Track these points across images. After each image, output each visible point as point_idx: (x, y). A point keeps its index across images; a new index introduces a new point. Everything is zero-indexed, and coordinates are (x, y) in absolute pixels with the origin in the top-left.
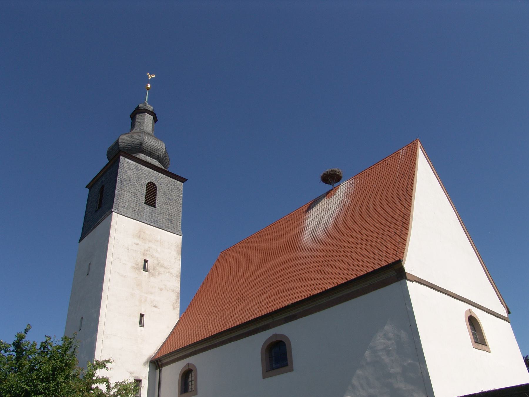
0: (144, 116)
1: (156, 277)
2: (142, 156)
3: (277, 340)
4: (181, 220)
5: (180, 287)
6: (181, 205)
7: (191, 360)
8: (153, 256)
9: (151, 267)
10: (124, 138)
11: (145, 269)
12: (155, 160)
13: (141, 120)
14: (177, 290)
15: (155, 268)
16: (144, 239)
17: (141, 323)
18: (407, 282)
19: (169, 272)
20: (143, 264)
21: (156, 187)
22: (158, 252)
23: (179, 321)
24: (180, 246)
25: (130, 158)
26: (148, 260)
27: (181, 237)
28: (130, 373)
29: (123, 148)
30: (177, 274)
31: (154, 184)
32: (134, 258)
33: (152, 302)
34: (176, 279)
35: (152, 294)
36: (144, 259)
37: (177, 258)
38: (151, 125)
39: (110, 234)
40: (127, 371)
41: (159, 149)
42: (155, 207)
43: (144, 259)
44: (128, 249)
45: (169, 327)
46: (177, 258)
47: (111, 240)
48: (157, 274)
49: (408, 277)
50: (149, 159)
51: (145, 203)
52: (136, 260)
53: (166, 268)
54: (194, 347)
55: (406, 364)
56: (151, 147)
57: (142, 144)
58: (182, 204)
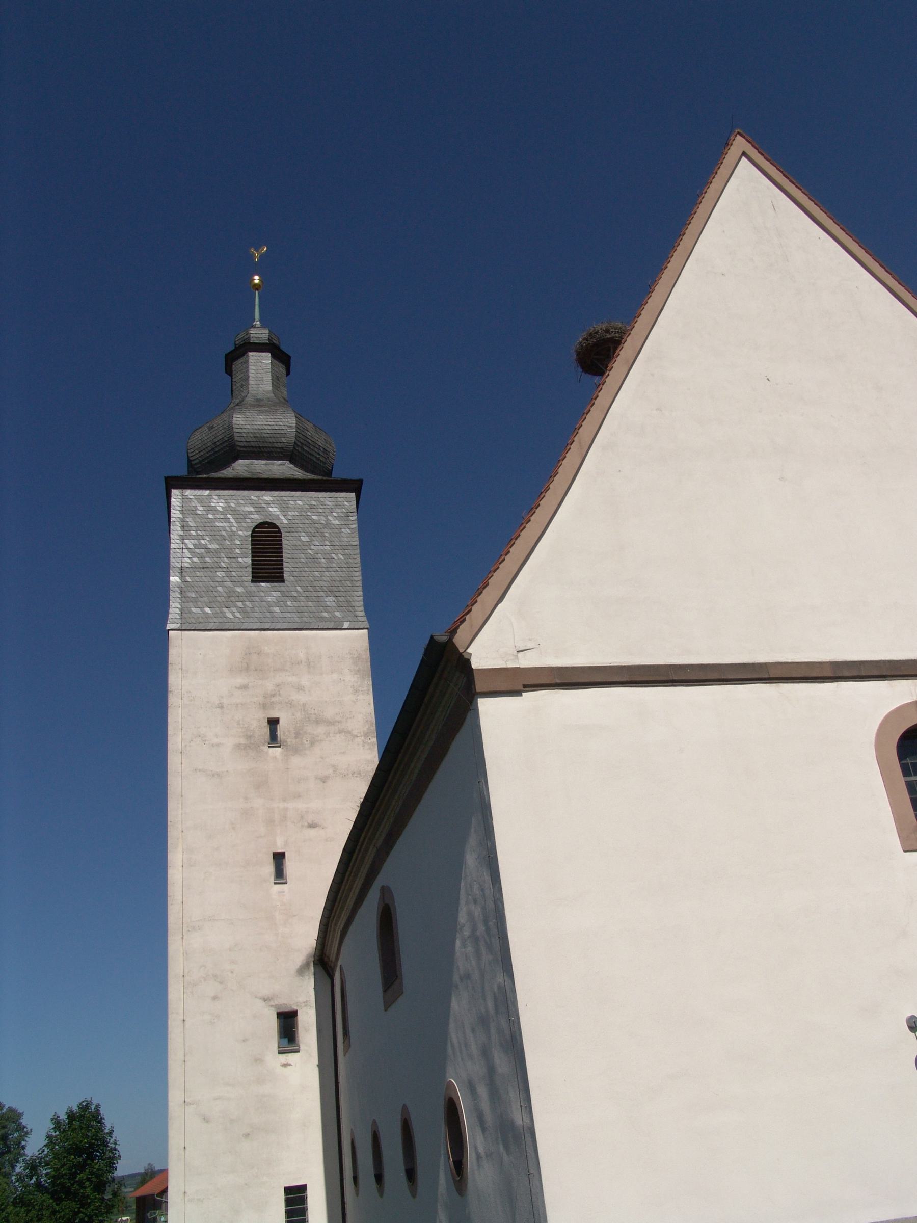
0: (247, 362)
8: (291, 704)
9: (289, 731)
10: (196, 437)
11: (274, 738)
12: (280, 462)
15: (301, 732)
16: (261, 670)
17: (280, 874)
19: (340, 732)
21: (280, 532)
22: (304, 690)
24: (367, 655)
26: (277, 717)
27: (367, 630)
29: (200, 462)
30: (365, 729)
32: (239, 724)
33: (302, 817)
35: (299, 796)
36: (268, 718)
37: (360, 689)
38: (268, 378)
39: (169, 685)
40: (256, 997)
41: (279, 432)
42: (283, 581)
43: (268, 718)
46: (360, 689)
47: (173, 700)
48: (307, 744)
52: (246, 725)
56: (258, 435)
57: (232, 437)
58: (358, 547)
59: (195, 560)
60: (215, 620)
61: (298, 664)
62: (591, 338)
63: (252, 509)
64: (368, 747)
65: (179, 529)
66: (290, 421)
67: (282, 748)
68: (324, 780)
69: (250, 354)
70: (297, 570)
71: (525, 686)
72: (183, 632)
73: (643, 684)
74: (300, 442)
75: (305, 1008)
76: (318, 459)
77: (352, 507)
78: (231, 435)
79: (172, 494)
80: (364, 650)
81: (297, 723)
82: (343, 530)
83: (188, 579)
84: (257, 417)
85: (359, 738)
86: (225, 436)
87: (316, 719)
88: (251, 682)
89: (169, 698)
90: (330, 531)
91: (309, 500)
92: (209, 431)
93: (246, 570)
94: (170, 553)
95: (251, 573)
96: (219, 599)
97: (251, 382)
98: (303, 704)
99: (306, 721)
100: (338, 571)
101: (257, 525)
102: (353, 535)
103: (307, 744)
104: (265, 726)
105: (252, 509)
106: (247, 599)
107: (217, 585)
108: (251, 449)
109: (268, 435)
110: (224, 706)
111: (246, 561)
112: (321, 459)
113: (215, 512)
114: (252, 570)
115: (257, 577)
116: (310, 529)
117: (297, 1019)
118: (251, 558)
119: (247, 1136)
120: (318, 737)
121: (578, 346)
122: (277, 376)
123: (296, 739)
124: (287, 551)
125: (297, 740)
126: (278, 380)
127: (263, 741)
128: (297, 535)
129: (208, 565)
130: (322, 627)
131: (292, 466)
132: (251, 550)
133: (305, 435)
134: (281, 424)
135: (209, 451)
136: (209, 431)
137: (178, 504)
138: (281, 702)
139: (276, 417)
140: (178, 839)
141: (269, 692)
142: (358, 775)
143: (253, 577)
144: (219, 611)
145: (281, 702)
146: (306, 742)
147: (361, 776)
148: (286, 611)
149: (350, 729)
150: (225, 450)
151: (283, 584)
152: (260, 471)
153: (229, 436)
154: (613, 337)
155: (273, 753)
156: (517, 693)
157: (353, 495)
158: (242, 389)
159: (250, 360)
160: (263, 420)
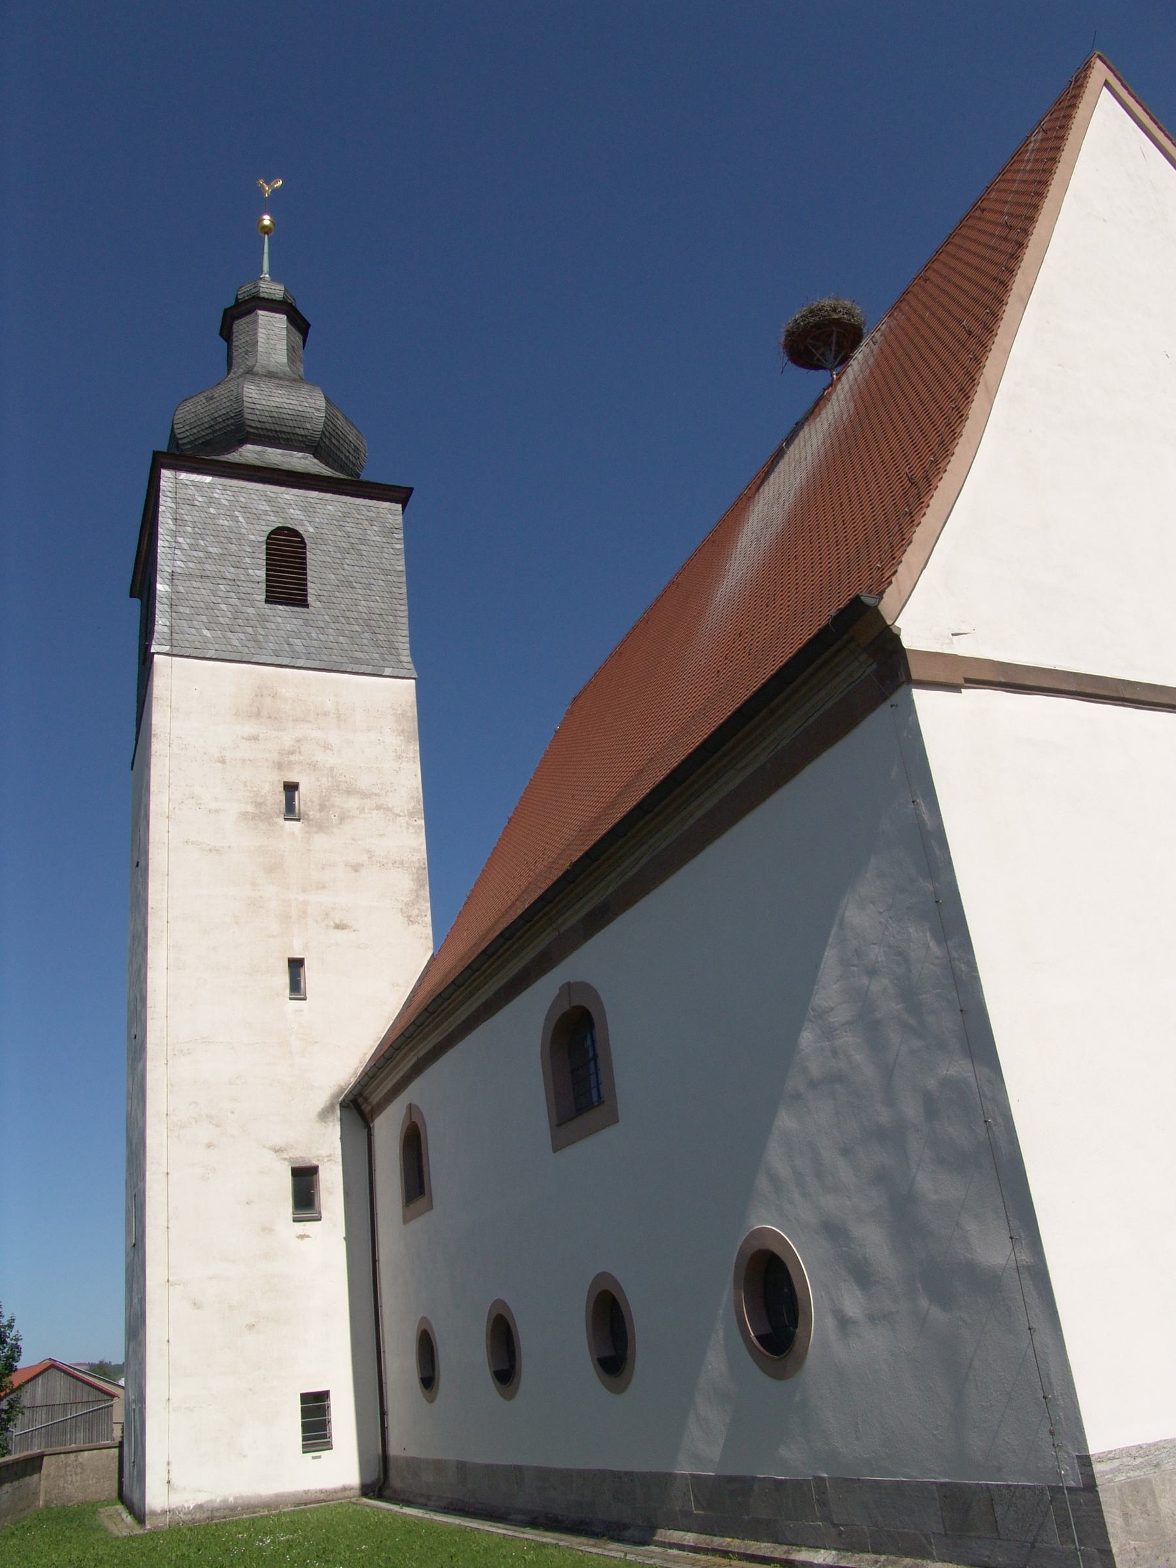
0: (256, 321)
1: (335, 830)
2: (249, 453)
3: (574, 1007)
4: (406, 627)
5: (424, 847)
6: (404, 579)
7: (413, 1093)
8: (314, 766)
9: (312, 801)
10: (187, 409)
11: (291, 810)
12: (301, 454)
13: (247, 338)
14: (415, 859)
15: (327, 803)
17: (296, 987)
18: (920, 697)
19: (378, 808)
20: (282, 797)
21: (303, 542)
22: (332, 750)
23: (433, 958)
24: (413, 712)
25: (196, 468)
27: (414, 681)
28: (276, 1152)
29: (191, 442)
30: (410, 807)
31: (297, 531)
32: (245, 785)
33: (327, 915)
34: (407, 823)
35: (324, 887)
36: (284, 782)
37: (404, 755)
38: (282, 346)
39: (153, 727)
41: (303, 414)
42: (307, 606)
43: (284, 782)
44: (223, 762)
45: (398, 985)
46: (404, 755)
48: (335, 820)
49: (915, 674)
50: (275, 456)
51: (267, 601)
52: (255, 789)
53: (365, 795)
54: (411, 1050)
55: (932, 1084)
56: (275, 414)
57: (240, 413)
58: (404, 573)
59: (191, 565)
60: (217, 646)
61: (325, 715)
62: (813, 316)
63: (268, 508)
64: (413, 831)
65: (170, 522)
66: (318, 402)
67: (302, 823)
68: (356, 868)
69: (260, 312)
70: (326, 594)
71: (967, 680)
72: (173, 658)
73: (1092, 698)
74: (329, 432)
75: (329, 1163)
76: (347, 458)
77: (397, 522)
78: (240, 409)
79: (162, 475)
80: (410, 706)
81: (322, 791)
82: (385, 550)
83: (181, 589)
84: (275, 391)
85: (401, 818)
86: (231, 411)
87: (347, 788)
88: (263, 733)
89: (152, 744)
90: (368, 548)
91: (343, 506)
92: (207, 401)
93: (259, 586)
94: (157, 552)
95: (265, 590)
96: (221, 619)
97: (260, 349)
98: (331, 767)
99: (335, 789)
100: (378, 602)
101: (274, 530)
102: (398, 558)
103: (335, 820)
104: (280, 792)
105: (268, 508)
106: (260, 624)
107: (220, 601)
108: (265, 432)
109: (288, 417)
110: (227, 761)
111: (259, 575)
112: (351, 459)
113: (219, 507)
114: (267, 587)
115: (272, 598)
116: (343, 543)
117: (317, 1180)
118: (265, 572)
119: (251, 1327)
120: (349, 811)
121: (791, 325)
122: (293, 347)
123: (321, 812)
124: (313, 568)
125: (322, 814)
126: (294, 352)
127: (278, 811)
128: (326, 549)
129: (208, 573)
130: (357, 671)
131: (316, 461)
132: (265, 561)
133: (335, 423)
134: (306, 405)
135: (206, 429)
136: (207, 401)
137: (170, 489)
138: (302, 762)
139: (299, 395)
140: (162, 932)
141: (286, 748)
142: (400, 866)
143: (267, 597)
144: (221, 636)
145: (302, 762)
146: (333, 817)
147: (404, 867)
148: (310, 645)
149: (390, 806)
150: (229, 429)
151: (306, 609)
152: (276, 462)
153: (237, 411)
154: (841, 318)
155: (290, 828)
156: (954, 687)
157: (399, 506)
158: (247, 357)
159: (260, 321)
160: (283, 396)
